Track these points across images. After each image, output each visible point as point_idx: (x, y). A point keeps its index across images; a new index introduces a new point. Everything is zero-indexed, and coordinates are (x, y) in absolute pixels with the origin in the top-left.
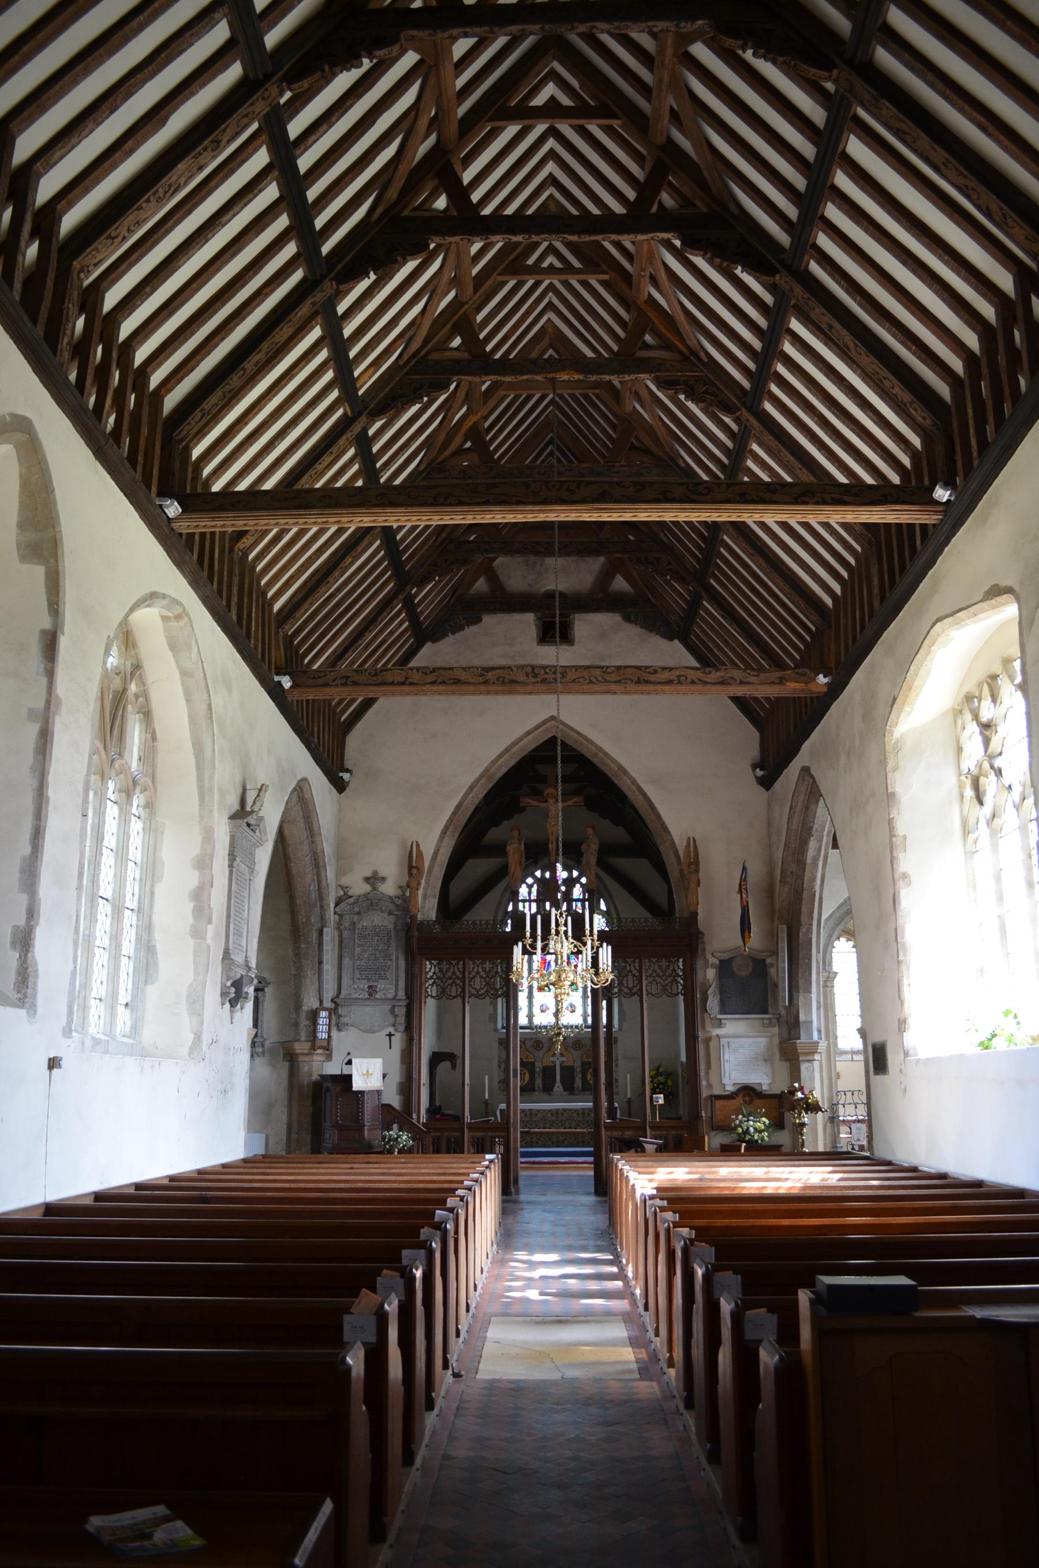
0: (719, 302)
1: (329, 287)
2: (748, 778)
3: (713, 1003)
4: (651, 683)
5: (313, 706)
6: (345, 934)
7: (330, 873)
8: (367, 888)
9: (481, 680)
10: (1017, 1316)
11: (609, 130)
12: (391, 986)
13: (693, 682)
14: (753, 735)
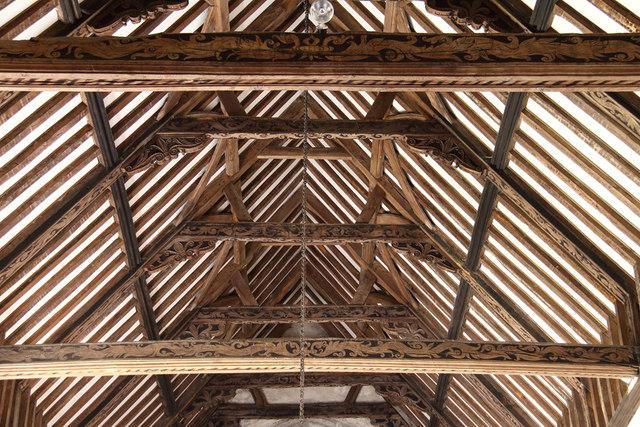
0: (450, 193)
1: (119, 170)
11: (349, 163)
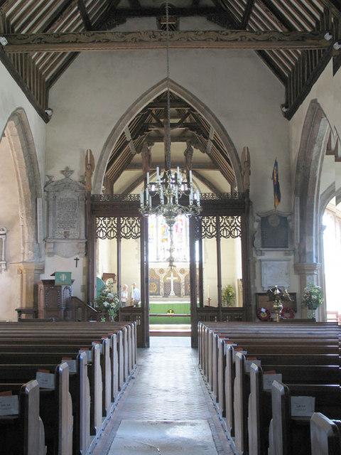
2: (279, 112)
3: (258, 242)
4: (226, 41)
5: (21, 57)
6: (51, 203)
7: (41, 167)
8: (62, 177)
9: (122, 40)
10: (85, 390)
12: (79, 230)
13: (250, 40)
14: (281, 88)
